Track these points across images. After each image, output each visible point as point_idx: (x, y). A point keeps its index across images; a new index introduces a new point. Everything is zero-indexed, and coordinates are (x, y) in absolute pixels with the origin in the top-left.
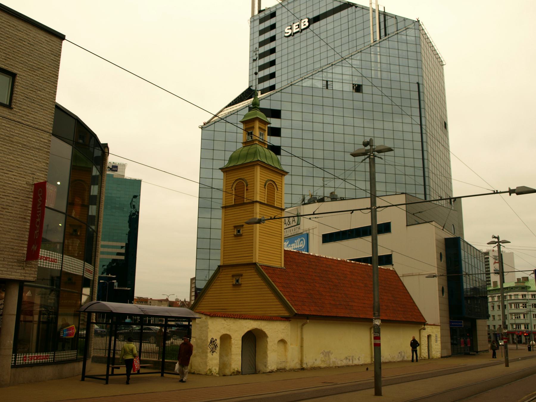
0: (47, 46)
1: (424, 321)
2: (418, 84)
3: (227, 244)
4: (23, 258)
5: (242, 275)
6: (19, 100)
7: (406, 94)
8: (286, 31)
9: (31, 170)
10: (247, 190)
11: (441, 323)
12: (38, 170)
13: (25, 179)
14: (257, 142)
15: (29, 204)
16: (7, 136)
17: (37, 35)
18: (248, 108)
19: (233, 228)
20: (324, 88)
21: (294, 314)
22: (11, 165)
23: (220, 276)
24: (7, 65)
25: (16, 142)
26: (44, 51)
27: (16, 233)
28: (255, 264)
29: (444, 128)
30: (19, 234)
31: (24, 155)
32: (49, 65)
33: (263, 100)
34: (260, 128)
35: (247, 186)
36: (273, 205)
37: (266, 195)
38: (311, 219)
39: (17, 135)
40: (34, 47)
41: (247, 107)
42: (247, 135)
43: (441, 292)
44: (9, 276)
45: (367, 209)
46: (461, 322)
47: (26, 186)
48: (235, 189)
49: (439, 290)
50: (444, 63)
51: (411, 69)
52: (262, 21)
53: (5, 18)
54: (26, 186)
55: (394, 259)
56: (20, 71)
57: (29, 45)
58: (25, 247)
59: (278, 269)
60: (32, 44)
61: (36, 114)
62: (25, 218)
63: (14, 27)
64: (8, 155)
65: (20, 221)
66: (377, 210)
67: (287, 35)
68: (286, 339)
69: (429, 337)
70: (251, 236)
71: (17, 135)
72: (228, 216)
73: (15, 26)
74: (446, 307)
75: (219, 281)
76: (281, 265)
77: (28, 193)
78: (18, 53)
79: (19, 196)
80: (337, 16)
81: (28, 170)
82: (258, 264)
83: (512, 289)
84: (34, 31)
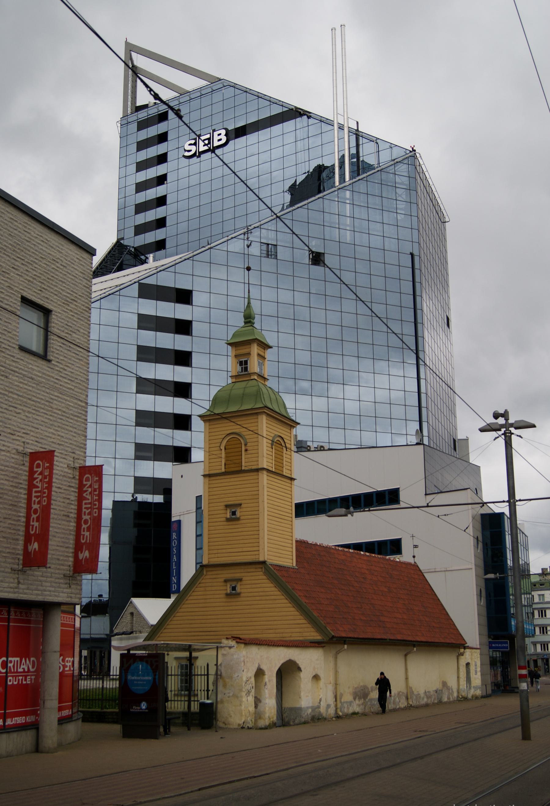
0: (79, 267)
1: (463, 643)
2: (412, 255)
3: (213, 532)
4: (68, 572)
5: (240, 580)
6: (56, 349)
7: (393, 271)
8: (187, 147)
9: (71, 448)
10: (246, 450)
11: (480, 644)
12: (78, 446)
13: (66, 461)
14: (256, 377)
15: (72, 495)
16: (47, 401)
17: (69, 252)
18: (137, 284)
19: (223, 507)
20: (262, 255)
21: (330, 637)
22: (53, 442)
23: (203, 581)
24: (43, 299)
25: (56, 409)
26: (76, 274)
27: (61, 538)
28: (264, 563)
29: (446, 326)
30: (63, 538)
31: (64, 426)
32: (81, 295)
33: (163, 271)
34: (259, 355)
35: (246, 445)
36: (281, 473)
37: (274, 459)
38: (440, 517)
39: (56, 398)
40: (67, 270)
41: (135, 282)
42: (238, 365)
43: (479, 597)
44: (56, 598)
45: (504, 502)
46: (506, 643)
47: (66, 470)
48: (225, 449)
49: (477, 595)
50: (447, 220)
51: (378, 218)
52: (142, 125)
53: (39, 231)
54: (66, 470)
55: (406, 547)
56: (55, 307)
57: (62, 267)
58: (70, 557)
59: (291, 570)
60: (65, 265)
61: (73, 367)
62: (68, 516)
63: (47, 242)
64: (49, 428)
65: (64, 520)
66: (517, 503)
67: (187, 154)
68: (322, 675)
69: (468, 664)
70: (255, 521)
71: (56, 398)
72: (215, 489)
73: (48, 241)
74: (485, 621)
75: (202, 589)
76: (293, 563)
77: (69, 480)
78: (53, 280)
79: (62, 485)
80: (277, 129)
81: (68, 447)
82: (268, 563)
83: (535, 585)
84: (65, 245)
